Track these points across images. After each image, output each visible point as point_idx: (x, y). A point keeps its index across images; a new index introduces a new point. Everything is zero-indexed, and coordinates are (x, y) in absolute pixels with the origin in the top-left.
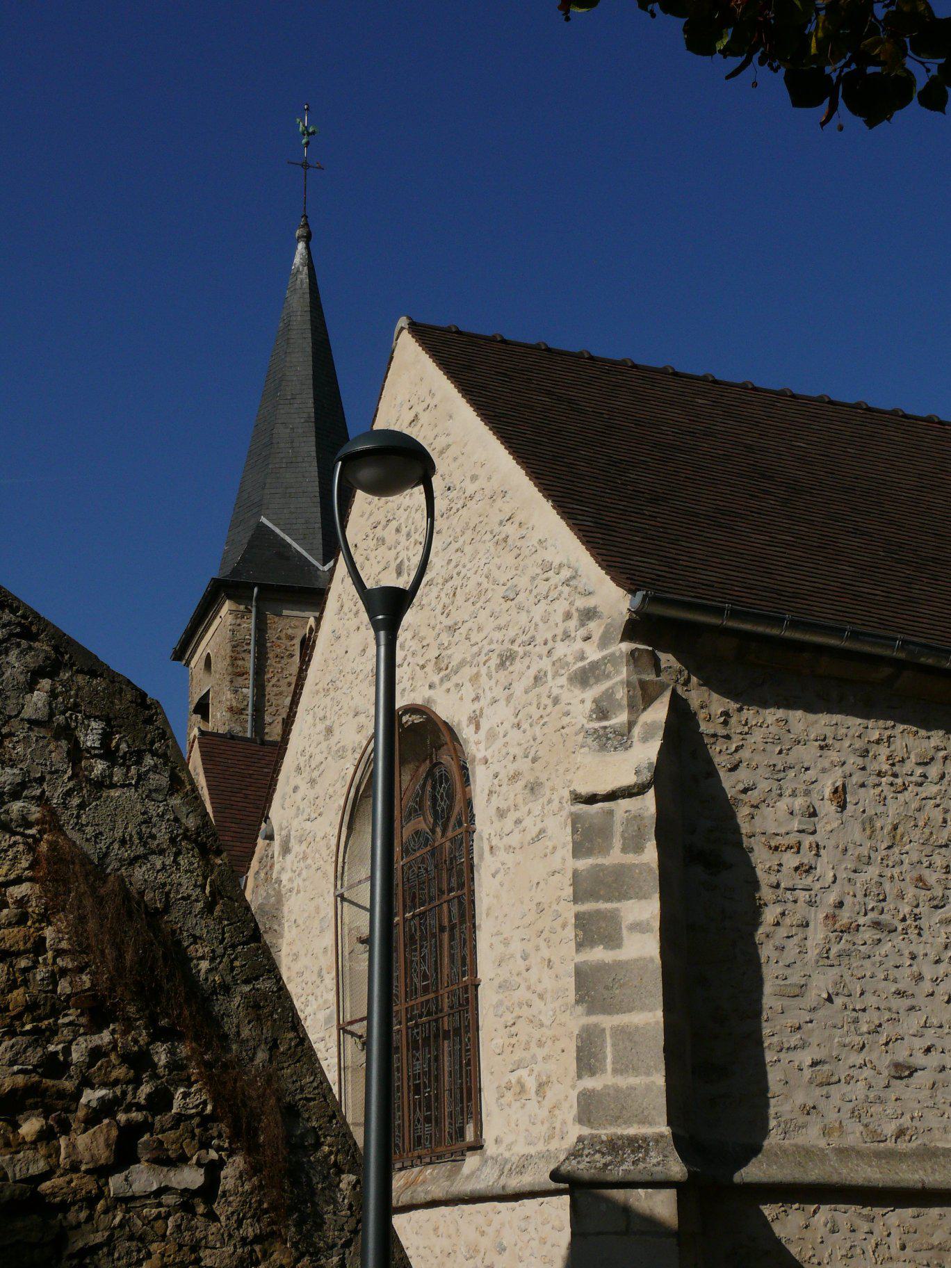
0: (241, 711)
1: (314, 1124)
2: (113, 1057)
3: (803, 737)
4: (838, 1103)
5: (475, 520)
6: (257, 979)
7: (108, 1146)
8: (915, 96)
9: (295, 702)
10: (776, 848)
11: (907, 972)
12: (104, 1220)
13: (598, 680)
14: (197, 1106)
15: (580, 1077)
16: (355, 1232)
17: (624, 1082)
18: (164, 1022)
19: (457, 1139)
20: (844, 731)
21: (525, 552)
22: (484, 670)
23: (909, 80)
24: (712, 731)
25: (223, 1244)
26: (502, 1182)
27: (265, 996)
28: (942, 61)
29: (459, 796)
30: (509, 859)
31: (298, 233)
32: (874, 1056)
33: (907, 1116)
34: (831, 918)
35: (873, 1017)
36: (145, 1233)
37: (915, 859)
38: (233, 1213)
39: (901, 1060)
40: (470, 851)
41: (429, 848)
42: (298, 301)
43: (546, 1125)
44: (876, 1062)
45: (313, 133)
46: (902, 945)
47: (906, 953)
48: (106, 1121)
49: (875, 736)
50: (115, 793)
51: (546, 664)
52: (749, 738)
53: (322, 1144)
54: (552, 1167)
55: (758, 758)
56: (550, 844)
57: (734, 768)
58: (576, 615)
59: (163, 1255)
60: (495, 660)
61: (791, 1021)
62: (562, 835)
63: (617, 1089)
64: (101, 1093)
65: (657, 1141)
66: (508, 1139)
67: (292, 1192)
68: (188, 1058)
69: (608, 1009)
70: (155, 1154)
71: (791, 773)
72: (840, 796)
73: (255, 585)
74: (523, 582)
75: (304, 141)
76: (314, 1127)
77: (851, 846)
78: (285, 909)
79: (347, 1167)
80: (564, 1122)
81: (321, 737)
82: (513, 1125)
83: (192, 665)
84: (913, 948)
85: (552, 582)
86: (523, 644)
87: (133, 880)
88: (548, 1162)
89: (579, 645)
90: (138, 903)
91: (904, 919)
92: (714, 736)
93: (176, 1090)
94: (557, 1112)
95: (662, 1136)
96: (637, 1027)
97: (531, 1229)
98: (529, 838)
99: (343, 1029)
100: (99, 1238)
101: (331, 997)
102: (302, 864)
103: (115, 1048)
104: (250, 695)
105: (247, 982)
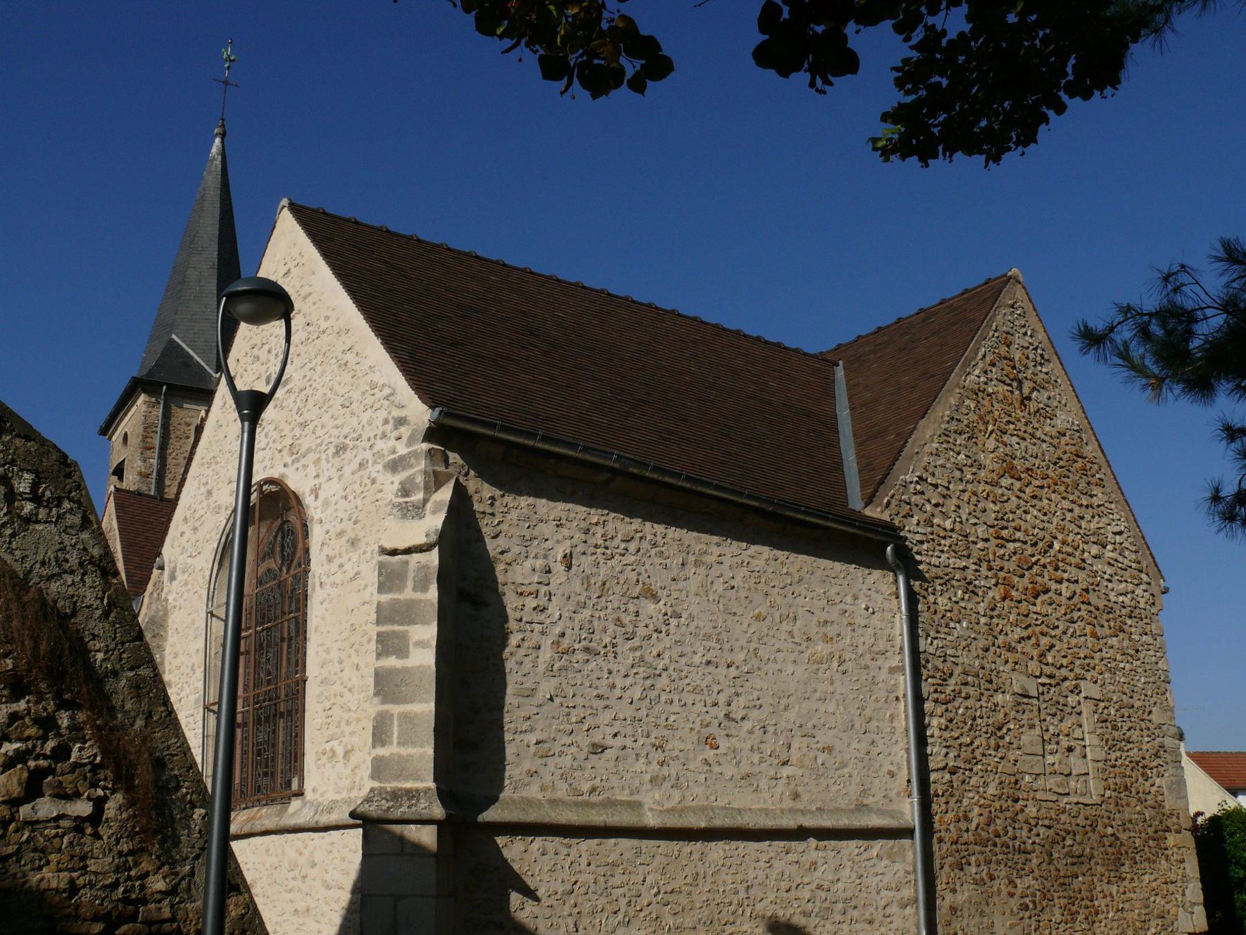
0: (148, 476)
1: (176, 772)
2: (27, 719)
3: (545, 517)
4: (553, 769)
5: (325, 349)
6: (139, 667)
7: (20, 784)
8: (625, 81)
9: (186, 471)
10: (521, 594)
11: (606, 682)
12: (15, 838)
13: (404, 468)
14: (89, 757)
15: (374, 747)
16: (203, 849)
17: (404, 751)
18: (67, 696)
19: (286, 788)
20: (574, 515)
21: (359, 374)
22: (324, 456)
23: (622, 72)
24: (482, 510)
25: (104, 855)
26: (316, 818)
27: (144, 680)
28: (643, 62)
29: (300, 546)
30: (333, 592)
31: (216, 131)
32: (579, 738)
33: (599, 779)
34: (556, 644)
35: (581, 712)
36: (46, 847)
37: (616, 606)
38: (113, 834)
39: (597, 741)
40: (306, 585)
41: (276, 581)
42: (212, 180)
43: (350, 780)
44: (579, 743)
45: (234, 60)
46: (603, 664)
47: (605, 670)
48: (19, 766)
49: (595, 520)
50: (39, 527)
51: (368, 455)
52: (509, 517)
53: (182, 787)
54: (351, 809)
55: (512, 531)
56: (363, 583)
57: (495, 537)
58: (391, 421)
59: (58, 863)
60: (332, 450)
61: (523, 713)
62: (371, 577)
63: (400, 756)
64: (18, 745)
65: (426, 793)
66: (321, 790)
67: (157, 820)
68: (84, 722)
69: (396, 700)
70: (56, 791)
71: (536, 542)
72: (568, 560)
73: (164, 384)
74: (356, 395)
75: (226, 65)
76: (176, 775)
77: (573, 595)
78: (170, 621)
79: (198, 804)
80: (362, 778)
81: (203, 498)
82: (326, 779)
83: (114, 439)
84: (610, 666)
85: (377, 396)
86: (353, 439)
87: (49, 591)
88: (349, 806)
89: (392, 443)
90: (52, 609)
91: (605, 647)
92: (484, 513)
93: (74, 745)
94: (357, 771)
95: (430, 789)
96: (416, 714)
97: (335, 851)
98: (348, 577)
99: (207, 708)
100: (11, 849)
101: (200, 685)
102: (184, 589)
103: (29, 713)
104: (155, 464)
105: (131, 669)
